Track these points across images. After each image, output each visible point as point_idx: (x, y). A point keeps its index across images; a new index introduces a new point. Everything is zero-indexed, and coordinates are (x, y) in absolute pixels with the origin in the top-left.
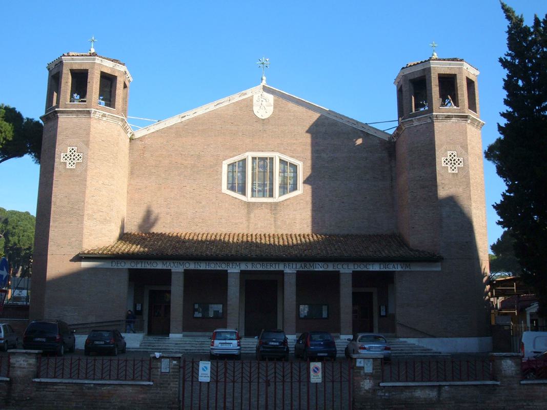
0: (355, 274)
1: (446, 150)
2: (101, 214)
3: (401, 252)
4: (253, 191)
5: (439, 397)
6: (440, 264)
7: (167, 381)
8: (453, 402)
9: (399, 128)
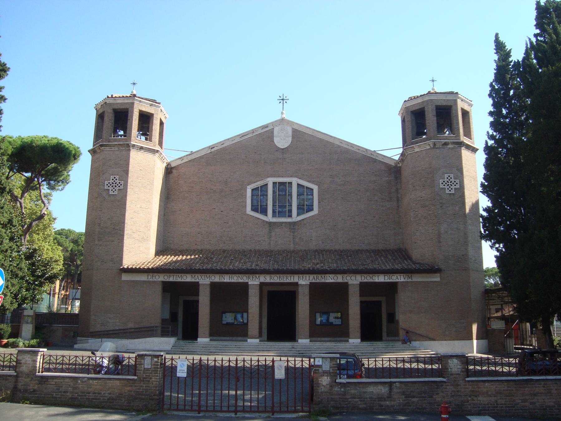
0: (363, 286)
1: (444, 174)
2: (138, 233)
3: (396, 266)
4: (274, 212)
5: (390, 392)
6: (439, 275)
7: (149, 376)
8: (404, 397)
9: (402, 154)
